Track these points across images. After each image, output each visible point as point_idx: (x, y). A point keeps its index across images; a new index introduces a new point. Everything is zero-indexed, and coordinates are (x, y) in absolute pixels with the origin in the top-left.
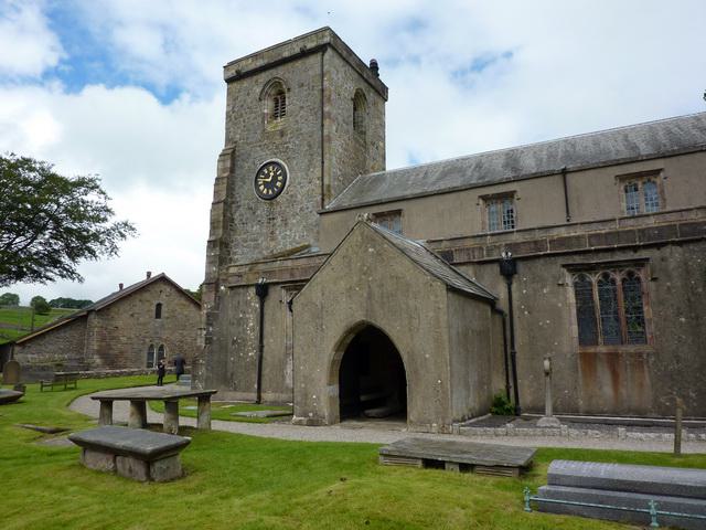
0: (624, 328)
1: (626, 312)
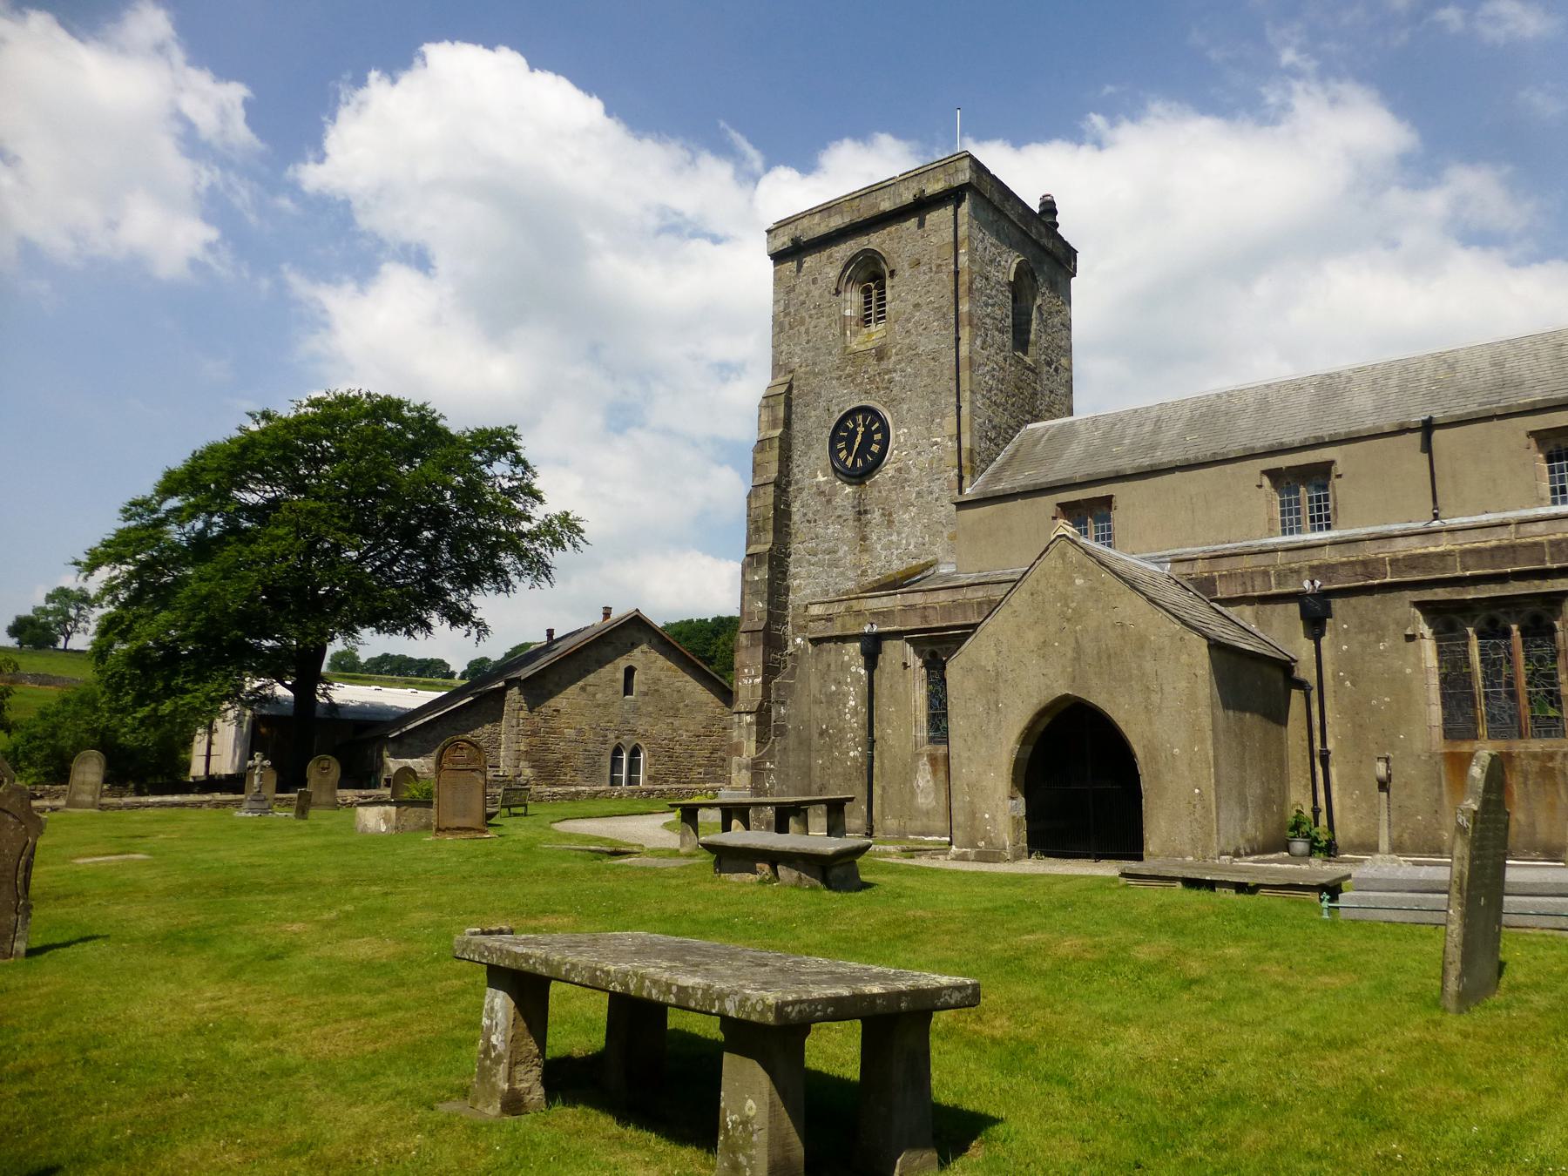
0: (1526, 712)
1: (1529, 683)
